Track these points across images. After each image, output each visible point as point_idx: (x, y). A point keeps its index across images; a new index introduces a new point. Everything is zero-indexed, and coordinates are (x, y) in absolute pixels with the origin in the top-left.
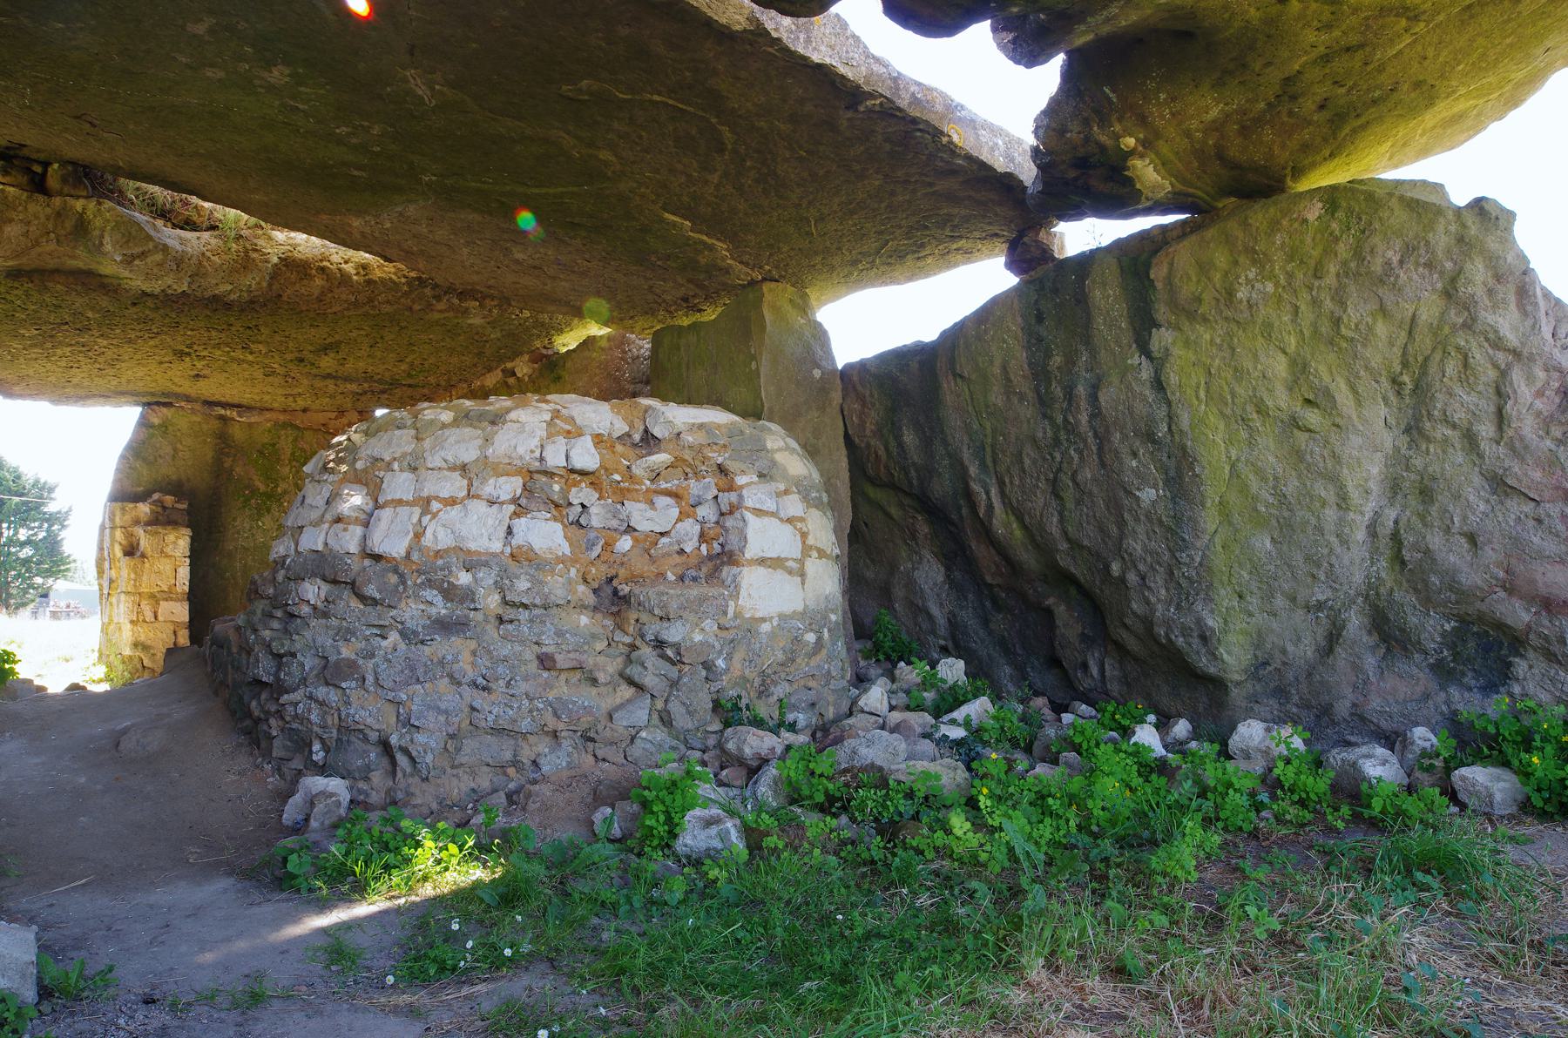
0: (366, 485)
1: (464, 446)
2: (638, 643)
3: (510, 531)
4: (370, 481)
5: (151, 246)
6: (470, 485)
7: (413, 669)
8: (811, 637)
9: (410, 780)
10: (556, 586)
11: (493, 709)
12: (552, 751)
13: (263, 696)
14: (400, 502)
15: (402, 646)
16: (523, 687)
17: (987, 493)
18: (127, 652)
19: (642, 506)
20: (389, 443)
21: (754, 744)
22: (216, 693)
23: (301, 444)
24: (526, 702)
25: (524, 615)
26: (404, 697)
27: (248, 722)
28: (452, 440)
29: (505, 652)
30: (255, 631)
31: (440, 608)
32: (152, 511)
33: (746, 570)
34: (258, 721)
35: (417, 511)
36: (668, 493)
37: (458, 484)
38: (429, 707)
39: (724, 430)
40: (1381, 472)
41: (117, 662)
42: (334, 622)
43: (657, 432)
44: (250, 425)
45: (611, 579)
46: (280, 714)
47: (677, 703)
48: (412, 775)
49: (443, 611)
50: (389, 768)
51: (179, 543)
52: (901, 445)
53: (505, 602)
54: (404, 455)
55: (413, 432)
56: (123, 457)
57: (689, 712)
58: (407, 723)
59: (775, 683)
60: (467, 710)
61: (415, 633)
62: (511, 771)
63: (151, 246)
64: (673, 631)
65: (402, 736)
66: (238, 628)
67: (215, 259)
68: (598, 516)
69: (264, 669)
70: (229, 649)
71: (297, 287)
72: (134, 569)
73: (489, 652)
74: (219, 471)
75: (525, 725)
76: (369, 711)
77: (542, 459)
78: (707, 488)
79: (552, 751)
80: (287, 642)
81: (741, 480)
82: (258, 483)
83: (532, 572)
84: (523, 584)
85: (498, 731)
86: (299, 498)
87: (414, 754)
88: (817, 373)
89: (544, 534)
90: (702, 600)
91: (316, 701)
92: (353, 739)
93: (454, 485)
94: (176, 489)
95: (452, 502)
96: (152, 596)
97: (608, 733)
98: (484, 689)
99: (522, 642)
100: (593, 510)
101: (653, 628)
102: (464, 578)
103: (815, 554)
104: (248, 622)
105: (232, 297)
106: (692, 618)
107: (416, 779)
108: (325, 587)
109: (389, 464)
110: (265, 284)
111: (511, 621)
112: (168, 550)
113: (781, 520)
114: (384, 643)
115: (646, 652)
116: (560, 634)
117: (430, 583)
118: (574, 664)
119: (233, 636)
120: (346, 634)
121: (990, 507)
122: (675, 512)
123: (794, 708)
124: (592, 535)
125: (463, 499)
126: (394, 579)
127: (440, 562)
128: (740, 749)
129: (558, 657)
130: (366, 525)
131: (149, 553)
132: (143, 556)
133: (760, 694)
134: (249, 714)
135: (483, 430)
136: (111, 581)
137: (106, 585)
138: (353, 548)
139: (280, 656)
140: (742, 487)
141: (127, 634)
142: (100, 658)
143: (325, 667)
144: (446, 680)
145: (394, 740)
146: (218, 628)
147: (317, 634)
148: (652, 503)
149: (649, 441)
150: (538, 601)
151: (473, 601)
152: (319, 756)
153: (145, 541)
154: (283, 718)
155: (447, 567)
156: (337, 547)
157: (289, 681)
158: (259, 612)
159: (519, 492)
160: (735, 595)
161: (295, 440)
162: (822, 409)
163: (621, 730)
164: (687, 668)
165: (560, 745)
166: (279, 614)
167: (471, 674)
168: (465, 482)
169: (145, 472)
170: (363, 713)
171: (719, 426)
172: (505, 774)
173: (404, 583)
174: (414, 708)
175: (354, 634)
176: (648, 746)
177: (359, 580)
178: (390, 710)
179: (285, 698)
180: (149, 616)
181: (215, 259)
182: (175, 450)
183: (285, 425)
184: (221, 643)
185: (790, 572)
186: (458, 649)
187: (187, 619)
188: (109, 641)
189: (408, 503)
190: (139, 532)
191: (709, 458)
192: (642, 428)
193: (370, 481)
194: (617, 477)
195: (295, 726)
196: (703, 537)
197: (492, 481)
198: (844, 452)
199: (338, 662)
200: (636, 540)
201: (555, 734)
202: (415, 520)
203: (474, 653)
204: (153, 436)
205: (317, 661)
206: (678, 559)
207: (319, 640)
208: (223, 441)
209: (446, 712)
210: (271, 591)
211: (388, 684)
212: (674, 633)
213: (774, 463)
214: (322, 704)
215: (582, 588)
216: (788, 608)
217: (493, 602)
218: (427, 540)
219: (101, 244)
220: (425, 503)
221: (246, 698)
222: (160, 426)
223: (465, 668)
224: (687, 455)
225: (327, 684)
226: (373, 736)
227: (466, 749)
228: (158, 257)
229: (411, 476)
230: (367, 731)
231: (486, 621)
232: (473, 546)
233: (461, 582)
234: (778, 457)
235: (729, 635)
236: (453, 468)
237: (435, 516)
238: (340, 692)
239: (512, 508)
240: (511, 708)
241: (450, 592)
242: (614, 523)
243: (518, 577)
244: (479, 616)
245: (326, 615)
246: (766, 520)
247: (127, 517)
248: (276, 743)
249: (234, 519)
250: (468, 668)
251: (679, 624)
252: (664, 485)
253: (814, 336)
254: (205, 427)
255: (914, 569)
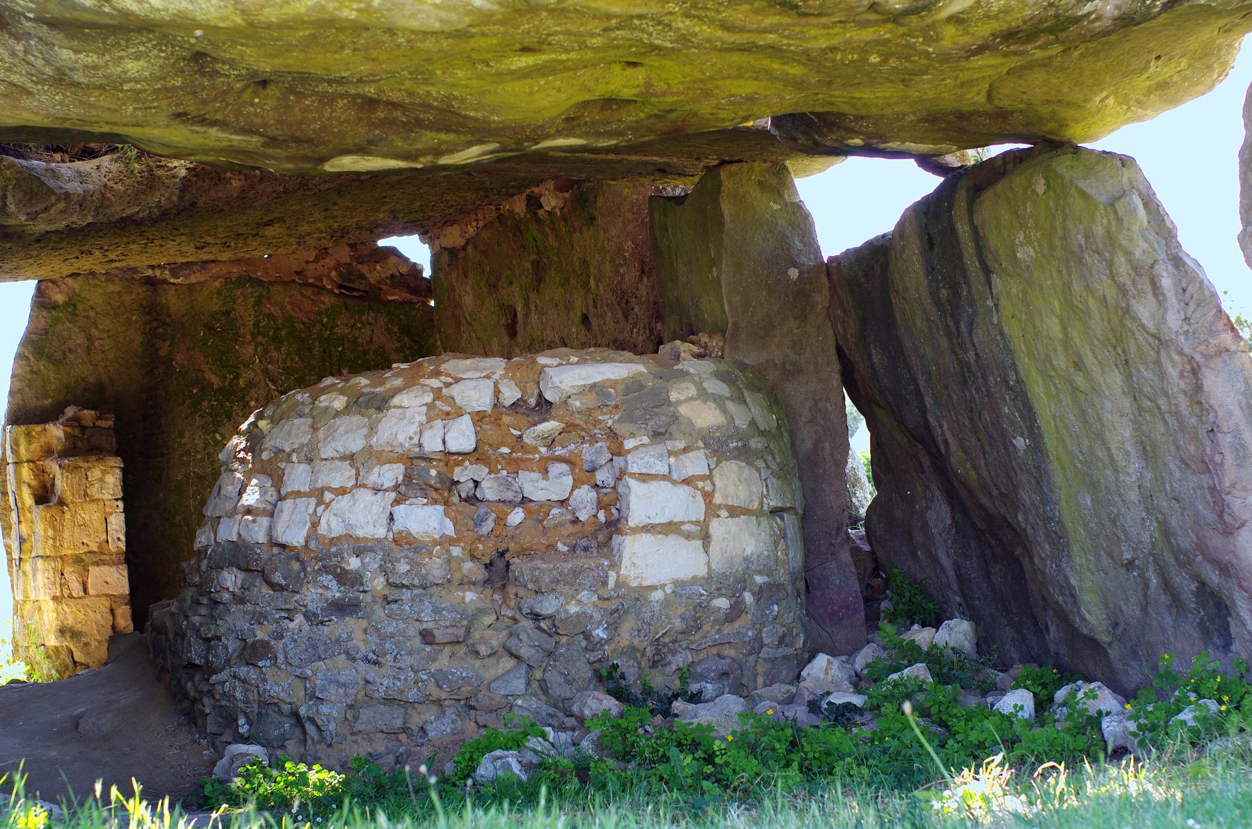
0: (271, 476)
1: (349, 436)
2: (518, 616)
3: (391, 518)
4: (272, 471)
5: (53, 199)
6: (358, 474)
7: (315, 647)
8: (723, 603)
9: (318, 747)
10: (435, 567)
11: (384, 681)
12: (438, 718)
13: (197, 678)
14: (298, 494)
15: (306, 628)
16: (408, 660)
17: (941, 427)
18: (52, 641)
19: (535, 476)
20: (289, 433)
21: (594, 706)
22: (159, 680)
23: (269, 308)
24: (411, 674)
25: (406, 595)
26: (309, 673)
27: (186, 704)
28: (342, 429)
29: (391, 629)
30: (187, 617)
31: (335, 592)
32: (67, 435)
33: (628, 539)
34: (194, 701)
35: (313, 501)
36: (561, 459)
37: (347, 474)
38: (331, 682)
39: (620, 388)
40: (1131, 435)
41: (39, 655)
42: (249, 607)
43: (549, 396)
44: (190, 287)
45: (502, 554)
46: (211, 693)
47: (555, 673)
48: (319, 743)
49: (338, 595)
50: (302, 737)
51: (107, 480)
52: (872, 365)
53: (390, 584)
54: (302, 446)
55: (310, 421)
56: (20, 357)
57: (567, 682)
58: (312, 696)
59: (674, 653)
60: (362, 683)
61: (315, 615)
62: (403, 737)
63: (53, 199)
64: (546, 604)
65: (309, 708)
66: (172, 615)
67: (119, 187)
68: (490, 490)
69: (195, 653)
70: (166, 635)
71: (212, 193)
72: (52, 523)
73: (377, 630)
74: (153, 363)
75: (412, 695)
76: (280, 685)
77: (420, 445)
78: (599, 452)
79: (438, 718)
80: (213, 627)
81: (629, 444)
82: (210, 376)
83: (411, 555)
84: (403, 567)
85: (389, 701)
86: (216, 488)
87: (320, 723)
88: (794, 273)
89: (425, 519)
90: (576, 573)
91: (239, 679)
92: (270, 712)
93: (342, 476)
94: (94, 396)
95: (342, 491)
96: (78, 560)
97: (487, 702)
98: (375, 663)
99: (405, 620)
100: (485, 484)
101: (529, 602)
102: (354, 563)
103: (724, 513)
104: (180, 609)
105: (141, 215)
106: (567, 590)
107: (323, 746)
108: (241, 575)
109: (289, 455)
110: (175, 198)
111: (396, 601)
112: (93, 491)
113: (674, 483)
114: (291, 625)
115: (527, 624)
116: (437, 611)
117: (326, 569)
118: (452, 638)
119: (168, 623)
120: (259, 618)
121: (946, 442)
122: (569, 480)
123: (703, 677)
124: (482, 510)
125: (352, 488)
126: (296, 566)
127: (334, 549)
128: (581, 711)
129: (436, 633)
130: (272, 515)
131: (69, 498)
132: (61, 502)
133: (654, 665)
134: (186, 696)
135: (369, 418)
136: (22, 541)
137: (15, 546)
138: (262, 538)
139: (208, 640)
140: (629, 452)
141: (49, 618)
142: (15, 651)
143: (244, 649)
144: (343, 656)
145: (303, 711)
146: (155, 614)
147: (237, 619)
148: (545, 472)
149: (544, 407)
150: (416, 582)
151: (362, 584)
152: (244, 729)
153: (62, 484)
154: (214, 697)
155: (339, 554)
156: (248, 538)
157: (216, 662)
158: (188, 599)
159: (401, 478)
160: (615, 565)
161: (258, 303)
162: (803, 317)
163: (498, 698)
164: (564, 639)
165: (444, 712)
166: (205, 601)
167: (363, 650)
168: (354, 471)
169: (52, 376)
170: (276, 688)
171: (613, 384)
172: (398, 740)
173: (304, 570)
174: (318, 682)
175: (266, 618)
176: (526, 713)
177: (267, 568)
178: (298, 684)
179: (214, 678)
180: (76, 589)
181: (119, 187)
182: (89, 338)
183: (242, 281)
184: (159, 630)
185: (688, 536)
186: (351, 628)
187: (126, 590)
188: (26, 626)
189: (306, 495)
190: (53, 467)
191: (600, 421)
192: (536, 392)
193: (272, 471)
194: (505, 450)
195: (223, 703)
196: (600, 505)
197: (376, 470)
198: (837, 366)
199: (254, 644)
200: (528, 512)
201: (438, 702)
202: (311, 511)
203: (365, 631)
204: (56, 321)
205: (238, 643)
206: (571, 529)
207: (239, 624)
208: (154, 313)
209: (345, 685)
210: (197, 579)
211: (296, 662)
212: (548, 606)
213: (675, 418)
214: (244, 682)
215: (468, 565)
216: (684, 574)
217: (379, 583)
218: (322, 529)
219: (5, 205)
220: (318, 494)
221: (183, 680)
222: (66, 305)
223: (361, 644)
224: (578, 420)
225: (248, 664)
226: (286, 709)
227: (363, 718)
228: (61, 206)
229: (308, 467)
230: (281, 705)
231: (374, 601)
232: (360, 533)
233: (351, 567)
234: (683, 410)
235: (613, 605)
236: (343, 458)
237: (328, 505)
238: (258, 670)
239: (393, 495)
240: (399, 679)
241: (343, 577)
242: (509, 495)
243: (398, 561)
244: (367, 598)
245: (242, 601)
246: (654, 485)
247: (35, 446)
248: (209, 720)
249: (181, 434)
250: (361, 644)
251: (551, 597)
252: (559, 451)
253: (791, 224)
254: (127, 299)
255: (928, 508)
